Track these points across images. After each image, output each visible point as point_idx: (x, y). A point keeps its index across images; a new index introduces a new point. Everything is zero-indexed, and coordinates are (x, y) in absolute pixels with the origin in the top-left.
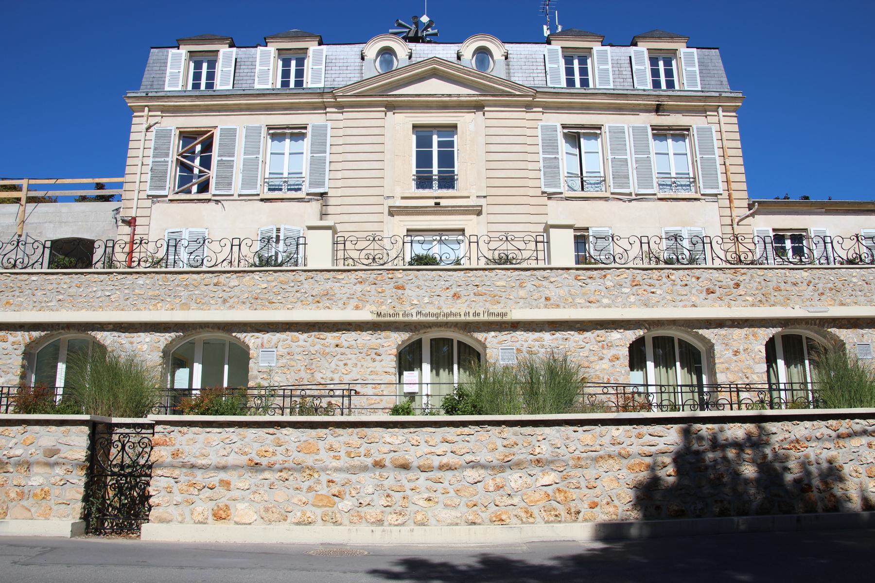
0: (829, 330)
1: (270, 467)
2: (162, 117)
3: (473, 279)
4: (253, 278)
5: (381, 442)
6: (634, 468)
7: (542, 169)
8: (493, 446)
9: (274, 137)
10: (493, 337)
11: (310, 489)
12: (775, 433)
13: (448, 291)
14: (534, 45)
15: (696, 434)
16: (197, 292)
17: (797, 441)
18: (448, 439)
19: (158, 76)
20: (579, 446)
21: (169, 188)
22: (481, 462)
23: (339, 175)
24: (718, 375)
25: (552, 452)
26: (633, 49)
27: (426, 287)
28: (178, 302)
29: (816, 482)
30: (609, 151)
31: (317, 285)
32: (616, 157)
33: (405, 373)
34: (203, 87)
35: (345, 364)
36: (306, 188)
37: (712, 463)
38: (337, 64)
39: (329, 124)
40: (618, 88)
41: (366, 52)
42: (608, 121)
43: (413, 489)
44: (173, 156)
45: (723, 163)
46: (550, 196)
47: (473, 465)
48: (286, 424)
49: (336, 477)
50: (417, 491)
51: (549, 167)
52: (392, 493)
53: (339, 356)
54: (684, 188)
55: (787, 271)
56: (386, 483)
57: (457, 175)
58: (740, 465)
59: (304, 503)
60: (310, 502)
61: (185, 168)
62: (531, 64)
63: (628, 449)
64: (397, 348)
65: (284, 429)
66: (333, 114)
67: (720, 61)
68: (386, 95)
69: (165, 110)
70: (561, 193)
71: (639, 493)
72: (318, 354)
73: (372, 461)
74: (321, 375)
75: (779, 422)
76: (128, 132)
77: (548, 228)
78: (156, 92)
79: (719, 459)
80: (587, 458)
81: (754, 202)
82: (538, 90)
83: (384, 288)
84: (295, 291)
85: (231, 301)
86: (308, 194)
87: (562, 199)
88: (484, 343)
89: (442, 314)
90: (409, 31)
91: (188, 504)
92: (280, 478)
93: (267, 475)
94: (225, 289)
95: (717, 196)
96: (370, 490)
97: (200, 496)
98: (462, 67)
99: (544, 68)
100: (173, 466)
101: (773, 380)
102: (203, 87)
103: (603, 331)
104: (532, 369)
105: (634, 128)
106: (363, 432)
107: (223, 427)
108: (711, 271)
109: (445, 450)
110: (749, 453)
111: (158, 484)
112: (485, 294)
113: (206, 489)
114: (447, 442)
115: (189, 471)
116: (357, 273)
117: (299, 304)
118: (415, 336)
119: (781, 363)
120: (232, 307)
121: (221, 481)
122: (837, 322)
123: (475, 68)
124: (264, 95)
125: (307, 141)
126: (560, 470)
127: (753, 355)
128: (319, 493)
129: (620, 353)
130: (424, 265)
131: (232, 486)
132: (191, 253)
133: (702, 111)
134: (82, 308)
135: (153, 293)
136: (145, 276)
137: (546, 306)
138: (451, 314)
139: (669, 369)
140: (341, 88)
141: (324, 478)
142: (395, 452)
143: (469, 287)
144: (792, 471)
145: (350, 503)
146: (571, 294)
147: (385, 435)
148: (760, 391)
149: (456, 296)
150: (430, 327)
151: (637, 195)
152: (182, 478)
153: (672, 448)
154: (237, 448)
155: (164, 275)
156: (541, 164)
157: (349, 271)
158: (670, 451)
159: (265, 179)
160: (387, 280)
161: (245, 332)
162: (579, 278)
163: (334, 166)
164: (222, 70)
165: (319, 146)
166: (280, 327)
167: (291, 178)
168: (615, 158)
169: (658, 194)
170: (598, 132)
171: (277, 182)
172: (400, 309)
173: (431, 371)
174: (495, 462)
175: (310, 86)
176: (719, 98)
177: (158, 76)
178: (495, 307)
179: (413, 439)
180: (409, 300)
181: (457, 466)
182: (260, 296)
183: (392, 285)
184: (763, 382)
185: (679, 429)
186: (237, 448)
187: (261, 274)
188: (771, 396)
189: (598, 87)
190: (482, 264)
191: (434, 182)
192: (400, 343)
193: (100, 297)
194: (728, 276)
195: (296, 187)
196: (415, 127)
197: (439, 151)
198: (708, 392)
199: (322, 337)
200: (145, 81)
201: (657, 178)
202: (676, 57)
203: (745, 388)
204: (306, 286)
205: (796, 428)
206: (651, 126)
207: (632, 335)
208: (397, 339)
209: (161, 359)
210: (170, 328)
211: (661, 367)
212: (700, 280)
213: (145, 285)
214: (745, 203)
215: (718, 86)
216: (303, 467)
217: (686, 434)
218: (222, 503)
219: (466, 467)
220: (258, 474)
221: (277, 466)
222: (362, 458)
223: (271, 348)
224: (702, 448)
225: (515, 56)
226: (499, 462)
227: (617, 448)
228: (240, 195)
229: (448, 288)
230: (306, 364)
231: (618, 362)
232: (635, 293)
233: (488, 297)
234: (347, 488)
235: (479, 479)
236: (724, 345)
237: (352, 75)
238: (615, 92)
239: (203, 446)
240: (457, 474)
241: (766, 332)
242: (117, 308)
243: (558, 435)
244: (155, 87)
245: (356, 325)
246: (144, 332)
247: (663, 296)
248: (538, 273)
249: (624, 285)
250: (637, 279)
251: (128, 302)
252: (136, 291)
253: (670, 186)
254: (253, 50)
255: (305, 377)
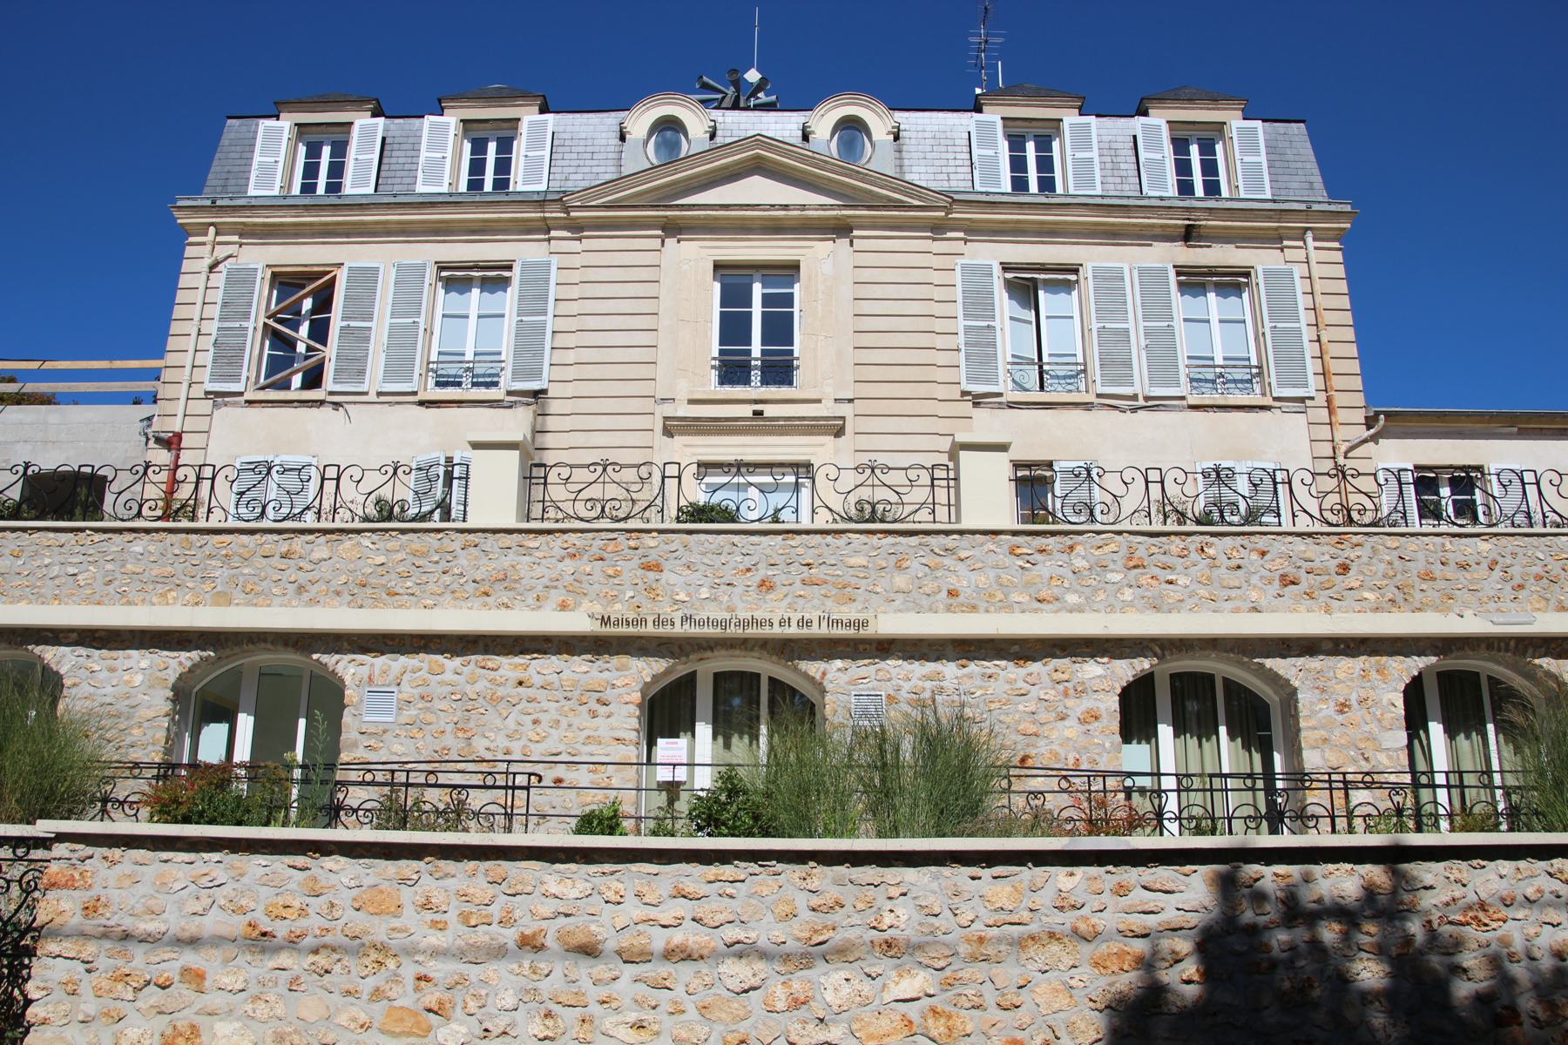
0: (1537, 661)
1: (293, 942)
2: (240, 246)
3: (800, 550)
4: (359, 544)
5: (537, 893)
6: (1108, 963)
7: (962, 347)
8: (788, 909)
9: (451, 284)
10: (839, 670)
11: (377, 994)
12: (1431, 887)
13: (749, 574)
14: (950, 115)
15: (1251, 886)
16: (246, 571)
17: (1483, 906)
18: (687, 890)
19: (237, 169)
20: (982, 912)
21: (248, 378)
22: (759, 943)
23: (570, 357)
24: (1306, 754)
25: (921, 924)
26: (1140, 121)
27: (703, 568)
28: (209, 589)
29: (1527, 1003)
30: (1093, 315)
31: (485, 560)
32: (1107, 325)
33: (661, 742)
34: (321, 190)
35: (535, 722)
36: (506, 382)
37: (1285, 954)
38: (573, 149)
39: (555, 260)
40: (1111, 193)
41: (629, 126)
42: (1092, 257)
43: (604, 1002)
44: (257, 318)
45: (1316, 338)
46: (977, 400)
47: (741, 950)
48: (333, 847)
49: (435, 968)
50: (614, 1005)
51: (976, 344)
52: (556, 1009)
53: (524, 704)
54: (1240, 386)
55: (1447, 541)
56: (545, 986)
57: (798, 359)
58: (1351, 959)
59: (362, 1026)
60: (376, 1024)
61: (282, 342)
62: (944, 149)
63: (1095, 919)
64: (643, 692)
65: (327, 858)
66: (563, 243)
67: (1308, 144)
68: (664, 206)
69: (247, 232)
70: (1000, 395)
71: (1116, 1021)
72: (481, 700)
73: (517, 936)
74: (486, 743)
75: (1438, 861)
76: (176, 272)
77: (957, 448)
78: (231, 199)
79: (1303, 945)
80: (999, 940)
81: (1377, 414)
82: (956, 197)
83: (619, 569)
84: (440, 571)
85: (314, 589)
86: (509, 393)
87: (1000, 406)
88: (821, 684)
89: (734, 621)
90: (723, 98)
91: (110, 1020)
92: (313, 967)
93: (284, 959)
94: (301, 565)
95: (1304, 402)
96: (509, 1000)
97: (138, 1004)
98: (810, 154)
99: (968, 156)
100: (84, 935)
101: (1421, 766)
102: (321, 190)
103: (1067, 661)
104: (884, 740)
105: (1142, 271)
106: (499, 870)
107: (198, 851)
108: (1290, 539)
109: (678, 914)
110: (1370, 932)
111: (48, 973)
112: (825, 582)
113: (152, 988)
114: (685, 897)
115: (119, 946)
116: (566, 537)
117: (448, 597)
118: (680, 667)
119: (1436, 729)
120: (314, 602)
121: (186, 971)
122: (1553, 645)
123: (835, 155)
124: (433, 204)
125: (513, 292)
126: (937, 966)
127: (1378, 713)
128: (395, 1003)
129: (1102, 706)
130: (706, 522)
131: (207, 983)
132: (243, 493)
133: (1275, 239)
134: (20, 599)
135: (160, 571)
136: (148, 537)
137: (949, 609)
138: (754, 621)
139: (1204, 740)
140: (579, 192)
141: (409, 971)
142: (567, 915)
143: (792, 568)
144: (1470, 974)
145: (464, 1030)
146: (1001, 585)
147: (546, 878)
148: (1396, 788)
149: (765, 585)
150: (712, 649)
151: (1147, 399)
152: (103, 963)
153: (1194, 919)
154: (225, 897)
155: (184, 535)
156: (961, 339)
157: (549, 532)
158: (1190, 925)
159: (428, 363)
160: (627, 551)
161: (337, 653)
162: (1018, 551)
163: (561, 340)
164: (357, 159)
165: (534, 302)
166: (1496, 645)
167: (479, 362)
168: (1104, 327)
169: (1189, 397)
170: (1073, 277)
171: (452, 370)
172: (649, 610)
173: (715, 737)
174: (792, 946)
175: (520, 188)
176: (1307, 214)
177: (237, 169)
178: (844, 608)
179: (609, 888)
180: (669, 593)
181: (705, 952)
182: (373, 581)
183: (636, 562)
184: (1400, 769)
185: (1211, 875)
186: (225, 897)
187: (375, 537)
188: (1417, 798)
189: (1071, 192)
190: (823, 520)
191: (752, 373)
192: (648, 679)
193: (57, 577)
194: (1326, 548)
195: (489, 380)
196: (718, 267)
197: (763, 313)
198: (1283, 790)
199: (490, 664)
200: (213, 179)
201: (1187, 366)
202: (1222, 137)
203: (1362, 782)
204: (463, 561)
205: (1479, 875)
206: (1174, 267)
207: (1126, 670)
208: (642, 671)
209: (169, 703)
210: (190, 642)
211: (1188, 735)
212: (1267, 557)
213: (146, 555)
214: (1359, 416)
215: (1306, 192)
216: (363, 945)
217: (1227, 886)
218: (183, 1020)
219: (724, 956)
220: (267, 956)
221: (308, 941)
222: (495, 928)
223: (388, 686)
224: (1262, 919)
225: (914, 135)
226: (799, 944)
227: (1069, 918)
228: (379, 394)
229: (749, 570)
230: (455, 720)
231: (1096, 724)
232: (1133, 583)
233: (831, 588)
234: (458, 995)
235: (755, 982)
236: (1317, 691)
237: (602, 169)
238: (1105, 201)
239: (152, 892)
240: (705, 971)
241: (1405, 666)
242: (87, 600)
243: (935, 886)
244: (230, 189)
245: (560, 641)
246: (137, 649)
247: (1191, 588)
248: (933, 540)
249: (1111, 566)
250: (1138, 554)
251: (110, 588)
252: (129, 567)
253: (1214, 382)
254: (417, 121)
255: (454, 745)
